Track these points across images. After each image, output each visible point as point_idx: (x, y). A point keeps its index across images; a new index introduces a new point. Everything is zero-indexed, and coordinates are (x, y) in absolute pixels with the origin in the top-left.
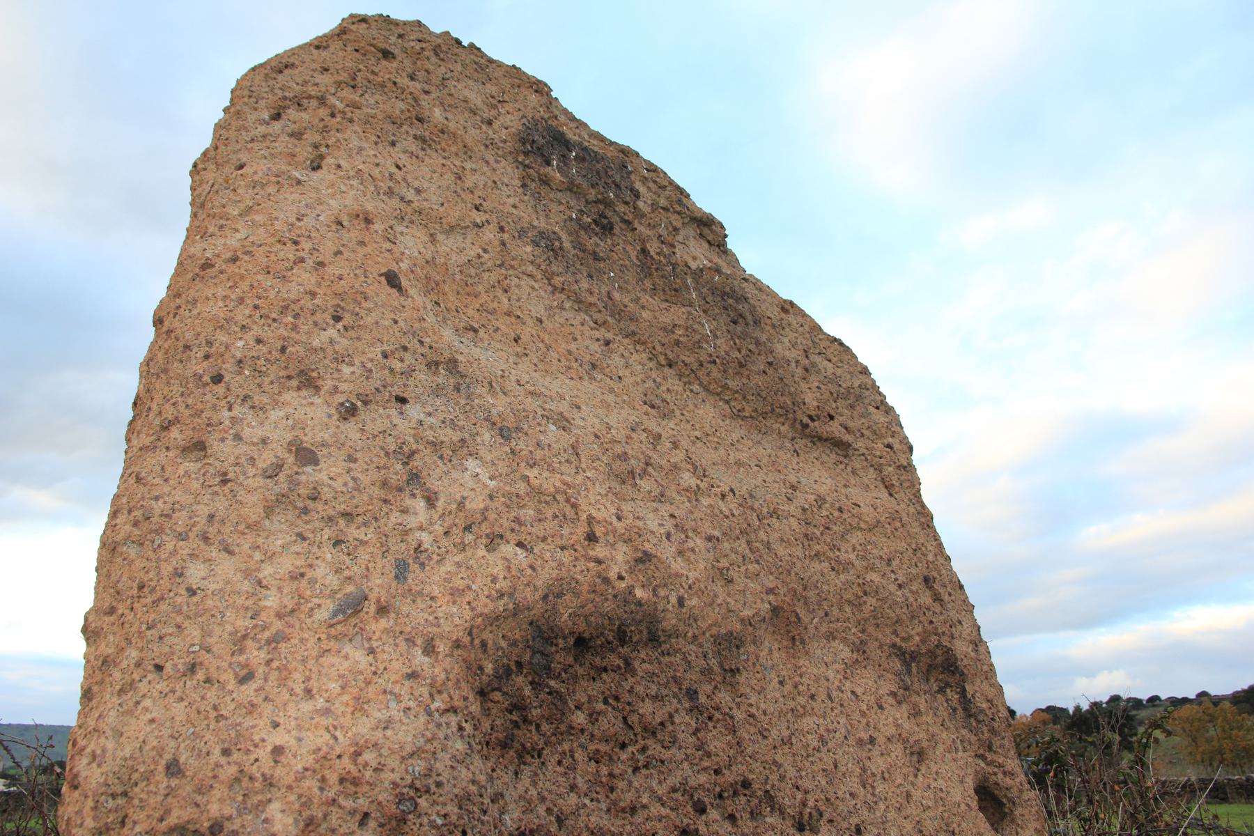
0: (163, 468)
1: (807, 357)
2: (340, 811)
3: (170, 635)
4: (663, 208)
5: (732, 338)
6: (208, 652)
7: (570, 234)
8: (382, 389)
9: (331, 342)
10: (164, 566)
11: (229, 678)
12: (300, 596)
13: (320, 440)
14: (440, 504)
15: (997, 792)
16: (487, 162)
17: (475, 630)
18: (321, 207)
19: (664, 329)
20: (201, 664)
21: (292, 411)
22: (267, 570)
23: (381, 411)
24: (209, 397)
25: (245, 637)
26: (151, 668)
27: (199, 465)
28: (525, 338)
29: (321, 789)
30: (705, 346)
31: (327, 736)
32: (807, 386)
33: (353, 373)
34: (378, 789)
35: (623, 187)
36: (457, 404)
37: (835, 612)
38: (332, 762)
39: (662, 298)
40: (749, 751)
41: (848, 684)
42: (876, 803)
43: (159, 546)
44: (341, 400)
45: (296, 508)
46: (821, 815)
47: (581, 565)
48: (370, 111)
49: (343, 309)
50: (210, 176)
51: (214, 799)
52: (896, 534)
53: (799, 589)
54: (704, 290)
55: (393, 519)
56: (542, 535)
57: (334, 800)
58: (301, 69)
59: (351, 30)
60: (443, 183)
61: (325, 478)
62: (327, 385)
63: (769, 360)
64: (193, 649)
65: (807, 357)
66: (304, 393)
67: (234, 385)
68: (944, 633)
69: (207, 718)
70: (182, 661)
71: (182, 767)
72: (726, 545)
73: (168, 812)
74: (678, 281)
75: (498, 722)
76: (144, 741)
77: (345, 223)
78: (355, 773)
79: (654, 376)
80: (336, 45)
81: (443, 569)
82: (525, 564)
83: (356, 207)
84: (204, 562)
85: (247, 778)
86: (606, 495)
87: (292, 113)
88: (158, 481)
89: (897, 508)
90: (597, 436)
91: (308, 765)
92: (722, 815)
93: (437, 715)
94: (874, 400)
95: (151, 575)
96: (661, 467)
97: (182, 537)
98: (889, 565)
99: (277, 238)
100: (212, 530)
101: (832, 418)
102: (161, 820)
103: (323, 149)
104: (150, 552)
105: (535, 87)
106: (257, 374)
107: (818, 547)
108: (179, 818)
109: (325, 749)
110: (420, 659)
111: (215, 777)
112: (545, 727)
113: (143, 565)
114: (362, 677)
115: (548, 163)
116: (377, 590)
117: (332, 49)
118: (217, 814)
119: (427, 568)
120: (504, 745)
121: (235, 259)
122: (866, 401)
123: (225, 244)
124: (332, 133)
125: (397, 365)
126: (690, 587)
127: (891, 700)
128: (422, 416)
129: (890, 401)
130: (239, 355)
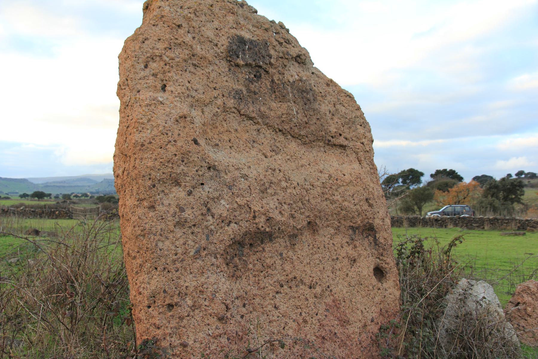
1: (335, 106)
14: (215, 217)
22: (177, 243)
30: (293, 120)
35: (265, 56)
40: (297, 268)
41: (331, 241)
46: (317, 284)
63: (318, 117)
65: (335, 106)
66: (177, 187)
72: (294, 205)
78: (203, 290)
79: (274, 137)
88: (144, 218)
101: (340, 135)
110: (214, 260)
112: (242, 270)
121: (150, 143)
127: (346, 244)
130: (159, 178)
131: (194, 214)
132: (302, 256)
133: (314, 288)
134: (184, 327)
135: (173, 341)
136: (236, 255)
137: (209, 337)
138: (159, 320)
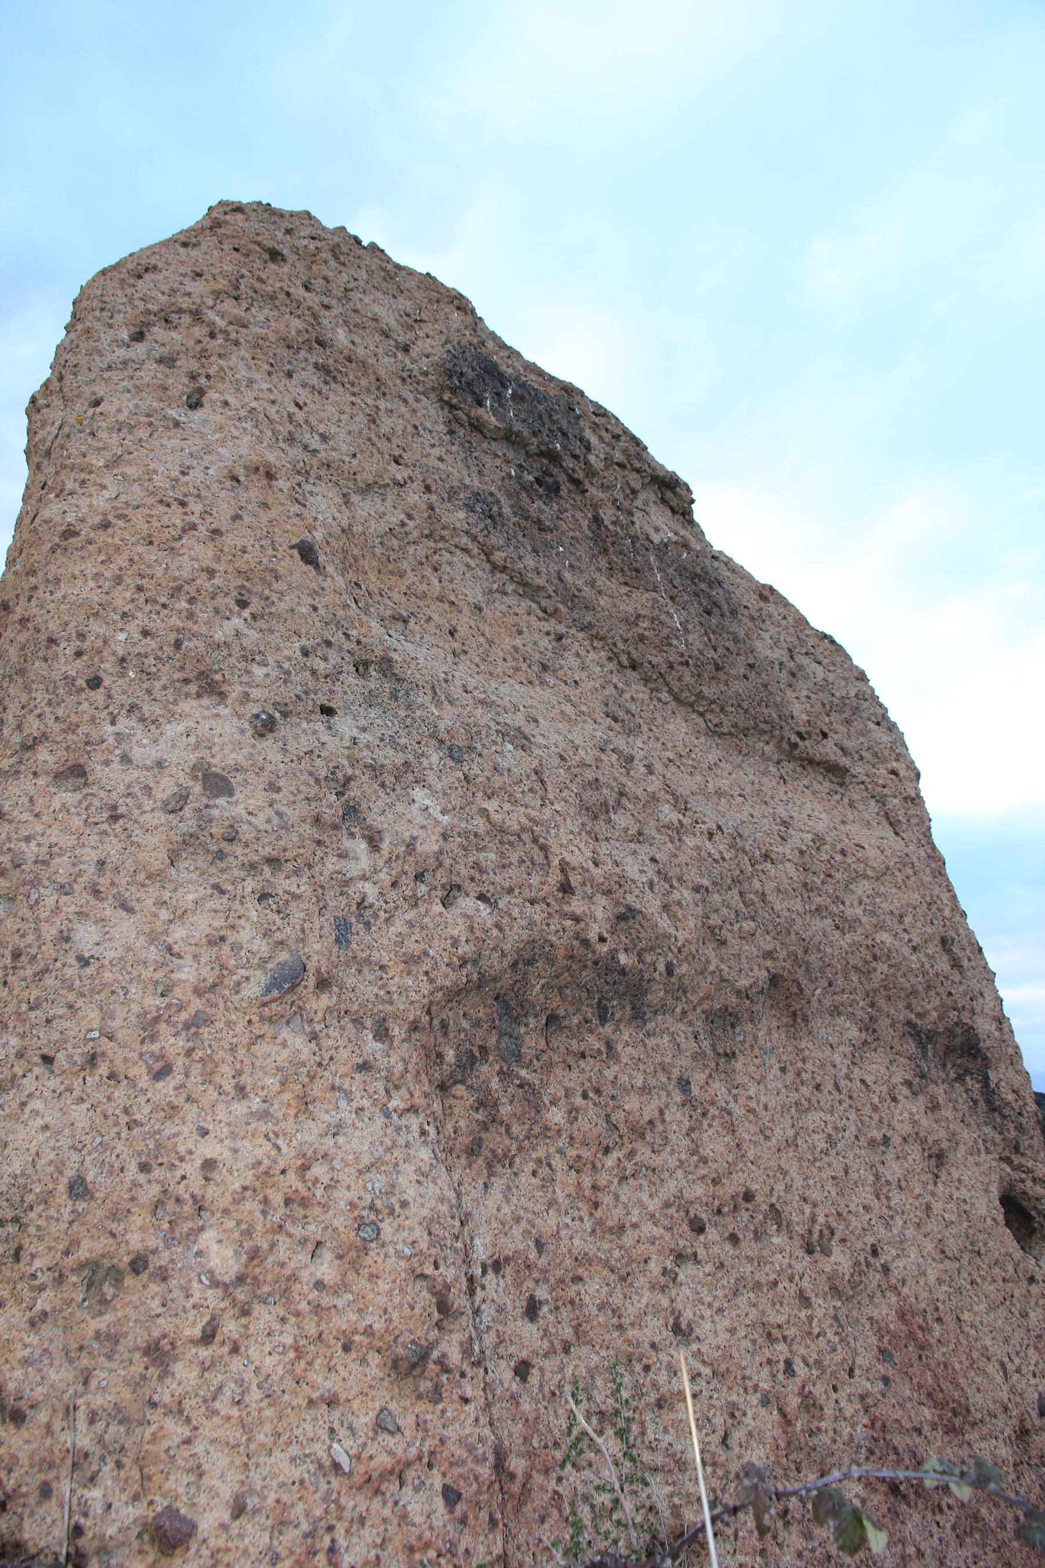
0: (31, 800)
1: (792, 657)
2: (288, 1240)
3: (61, 1017)
4: (618, 464)
5: (706, 634)
6: (110, 1039)
7: (509, 496)
8: (303, 696)
9: (238, 634)
10: (45, 928)
11: (139, 1071)
12: (222, 967)
13: (233, 763)
14: (385, 846)
15: (1025, 1203)
16: (405, 401)
17: (434, 1008)
18: (210, 457)
19: (626, 621)
20: (103, 1054)
21: (194, 725)
22: (178, 934)
23: (304, 725)
24: (85, 706)
25: (157, 1019)
26: (37, 1059)
27: (79, 796)
28: (462, 631)
29: (264, 1213)
30: (675, 642)
31: (268, 1146)
32: (794, 695)
33: (267, 675)
34: (331, 1212)
36: (396, 716)
37: (840, 982)
38: (276, 1179)
39: (622, 580)
41: (856, 1070)
42: (892, 1217)
43: (37, 902)
44: (255, 711)
45: (208, 851)
46: (833, 1234)
47: (555, 924)
48: (259, 330)
49: (249, 591)
50: (56, 414)
51: (133, 1227)
52: (908, 883)
53: (800, 952)
54: (671, 571)
55: (330, 866)
56: (507, 885)
57: (281, 1227)
58: (167, 274)
59: (227, 223)
60: (355, 427)
61: (243, 812)
62: (235, 691)
64: (92, 1035)
65: (792, 657)
66: (206, 701)
67: (116, 690)
68: (963, 1007)
69: (116, 1124)
70: (79, 1050)
71: (90, 1187)
72: (716, 897)
73: (76, 1243)
74: (639, 559)
75: (462, 1124)
76: (37, 1154)
77: (242, 479)
78: (304, 1192)
80: (208, 242)
81: (392, 929)
82: (489, 923)
83: (255, 458)
84: (96, 923)
85: (172, 1201)
86: (580, 834)
87: (158, 332)
88: (26, 816)
89: (906, 850)
90: (562, 758)
91: (247, 1183)
92: (721, 1235)
93: (395, 1116)
94: (875, 714)
95: (30, 938)
96: (637, 798)
97: (64, 889)
98: (901, 922)
99: (158, 498)
100: (104, 881)
101: (825, 735)
102: (67, 1253)
103: (203, 381)
104: (25, 910)
105: (456, 302)
106: (144, 677)
107: (819, 899)
108: (91, 1251)
109: (266, 1162)
110: (372, 1046)
111: (133, 1199)
113: (16, 927)
114: (304, 1070)
115: (480, 403)
116: (315, 958)
117: (204, 247)
118: (139, 1247)
119: (373, 928)
120: (472, 1152)
121: (105, 525)
122: (865, 715)
123: (90, 506)
124: (213, 359)
125: (321, 666)
126: (679, 951)
127: (905, 1091)
128: (355, 732)
129: (892, 716)
130: (121, 652)
131: (280, 814)
132: (766, 1107)
133: (827, 1252)
134: (178, 1410)
135: (98, 1508)
136: (483, 1049)
137: (335, 1483)
138: (26, 1362)
